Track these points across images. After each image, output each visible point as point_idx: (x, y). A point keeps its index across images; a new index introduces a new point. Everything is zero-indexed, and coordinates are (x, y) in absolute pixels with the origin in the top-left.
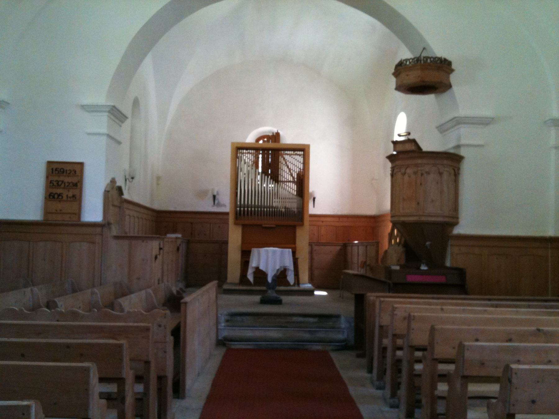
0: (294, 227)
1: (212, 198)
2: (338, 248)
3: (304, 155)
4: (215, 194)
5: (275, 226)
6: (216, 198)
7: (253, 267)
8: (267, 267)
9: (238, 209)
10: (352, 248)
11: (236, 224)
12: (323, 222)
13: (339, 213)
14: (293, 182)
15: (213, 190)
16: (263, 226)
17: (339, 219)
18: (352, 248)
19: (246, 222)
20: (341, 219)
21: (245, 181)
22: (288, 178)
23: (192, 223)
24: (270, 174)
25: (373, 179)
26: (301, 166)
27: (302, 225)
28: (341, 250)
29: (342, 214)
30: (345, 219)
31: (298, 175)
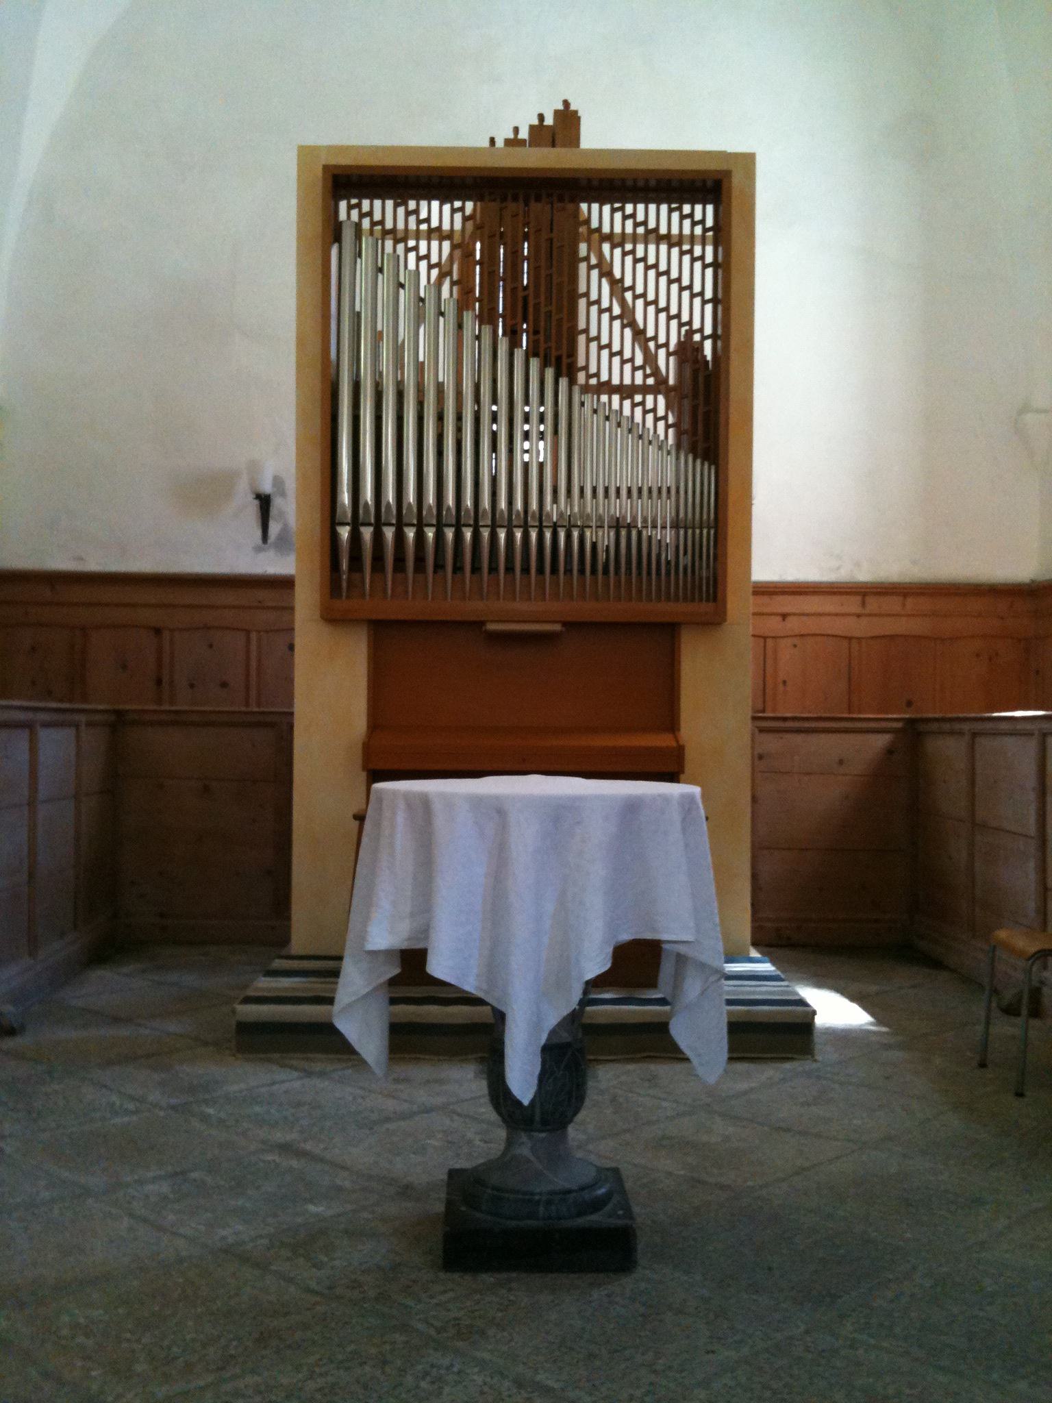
0: (669, 631)
1: (253, 507)
2: (882, 741)
3: (721, 234)
4: (267, 487)
5: (557, 627)
6: (273, 511)
7: (374, 954)
8: (494, 965)
9: (345, 532)
10: (972, 747)
11: (333, 617)
12: (784, 616)
13: (864, 575)
14: (660, 386)
15: (254, 468)
16: (491, 627)
17: (863, 604)
18: (972, 747)
19: (392, 609)
20: (873, 604)
21: (400, 395)
22: (675, 216)
23: (158, 631)
24: (527, 258)
25: (1025, 409)
26: (704, 318)
27: (715, 619)
28: (890, 751)
29: (879, 580)
30: (893, 604)
31: (687, 351)
